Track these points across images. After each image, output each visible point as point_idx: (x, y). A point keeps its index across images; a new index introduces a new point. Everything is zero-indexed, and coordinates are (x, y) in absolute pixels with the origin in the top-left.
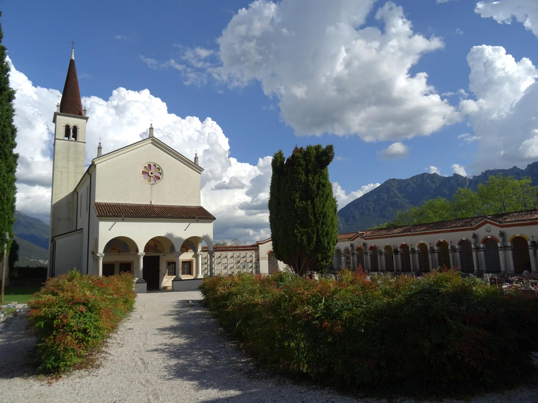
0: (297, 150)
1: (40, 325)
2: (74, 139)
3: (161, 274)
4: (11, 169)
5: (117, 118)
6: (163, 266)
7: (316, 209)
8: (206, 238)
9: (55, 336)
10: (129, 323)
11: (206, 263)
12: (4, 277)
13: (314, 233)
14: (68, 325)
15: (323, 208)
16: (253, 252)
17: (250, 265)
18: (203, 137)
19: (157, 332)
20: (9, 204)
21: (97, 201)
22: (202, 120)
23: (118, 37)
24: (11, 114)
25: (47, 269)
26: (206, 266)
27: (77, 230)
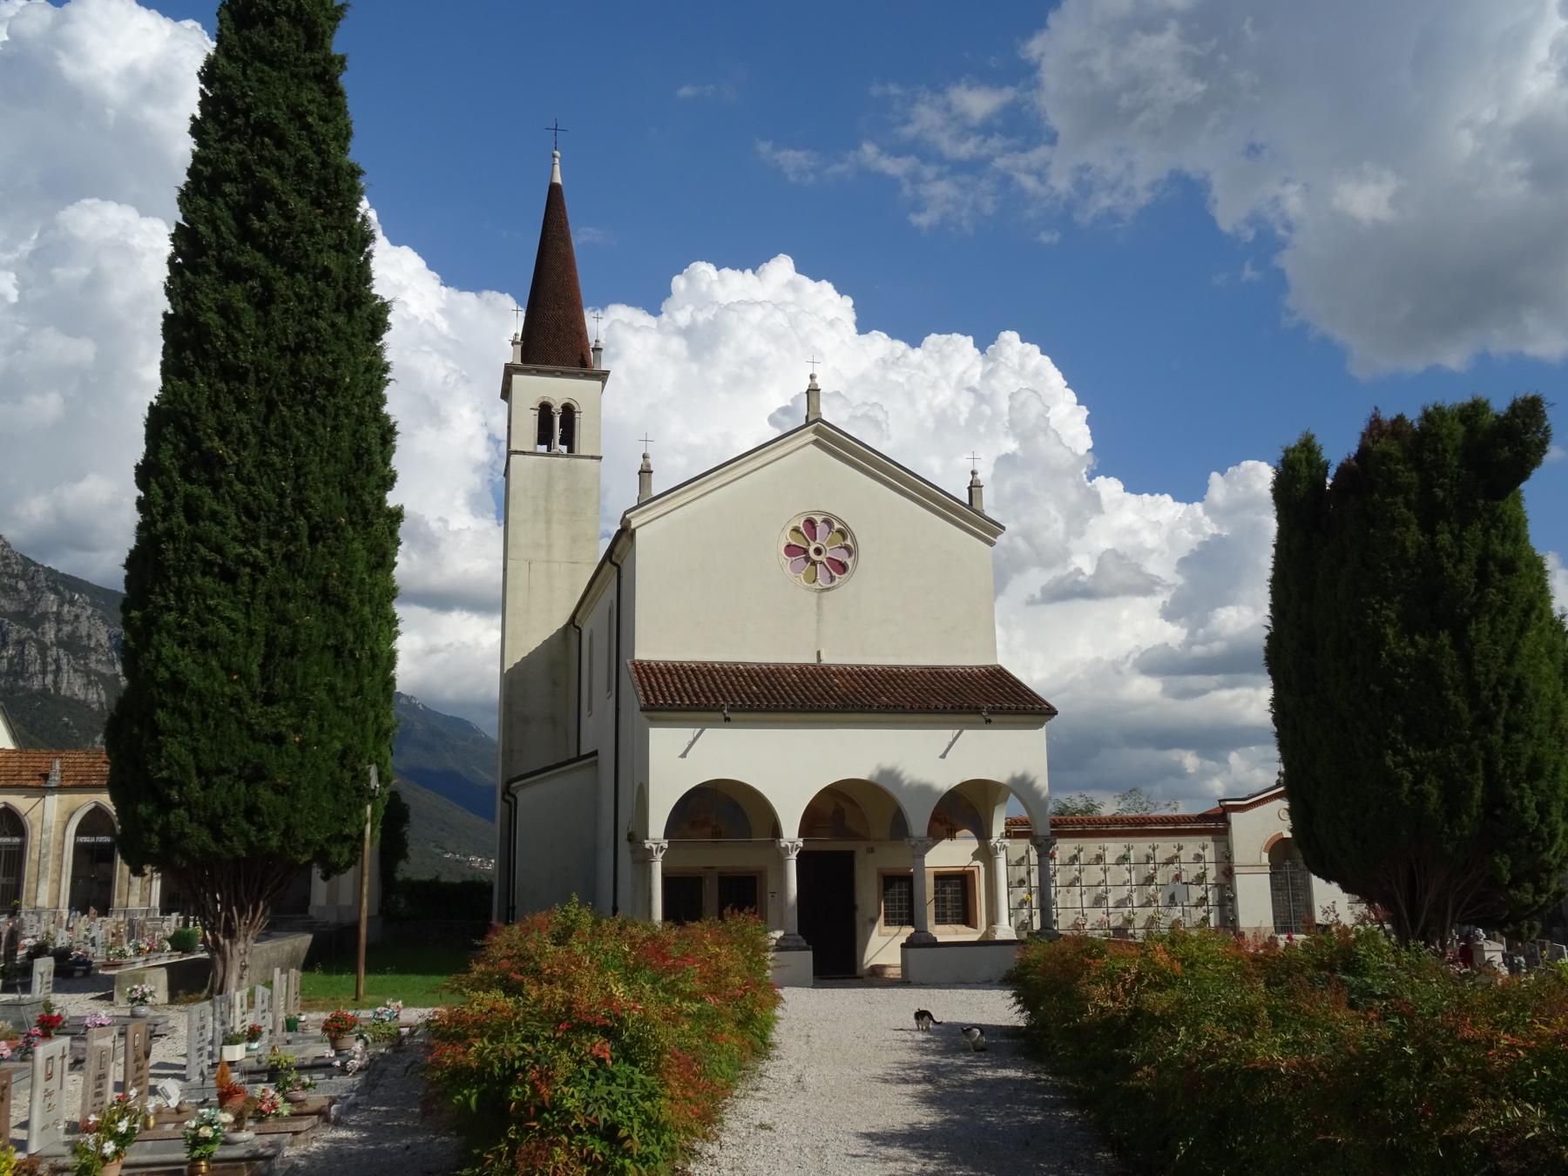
0: (1376, 428)
1: (467, 1099)
2: (564, 449)
3: (860, 919)
4: (383, 561)
5: (694, 368)
6: (867, 891)
8: (1021, 787)
9: (513, 1144)
10: (760, 1104)
11: (1021, 882)
12: (364, 915)
13: (1472, 768)
14: (555, 1106)
15: (1510, 660)
16: (1208, 840)
17: (1196, 892)
18: (987, 410)
19: (860, 1147)
20: (377, 672)
21: (641, 655)
22: (984, 342)
23: (686, 91)
24: (380, 378)
25: (491, 887)
26: (1022, 893)
27: (580, 758)
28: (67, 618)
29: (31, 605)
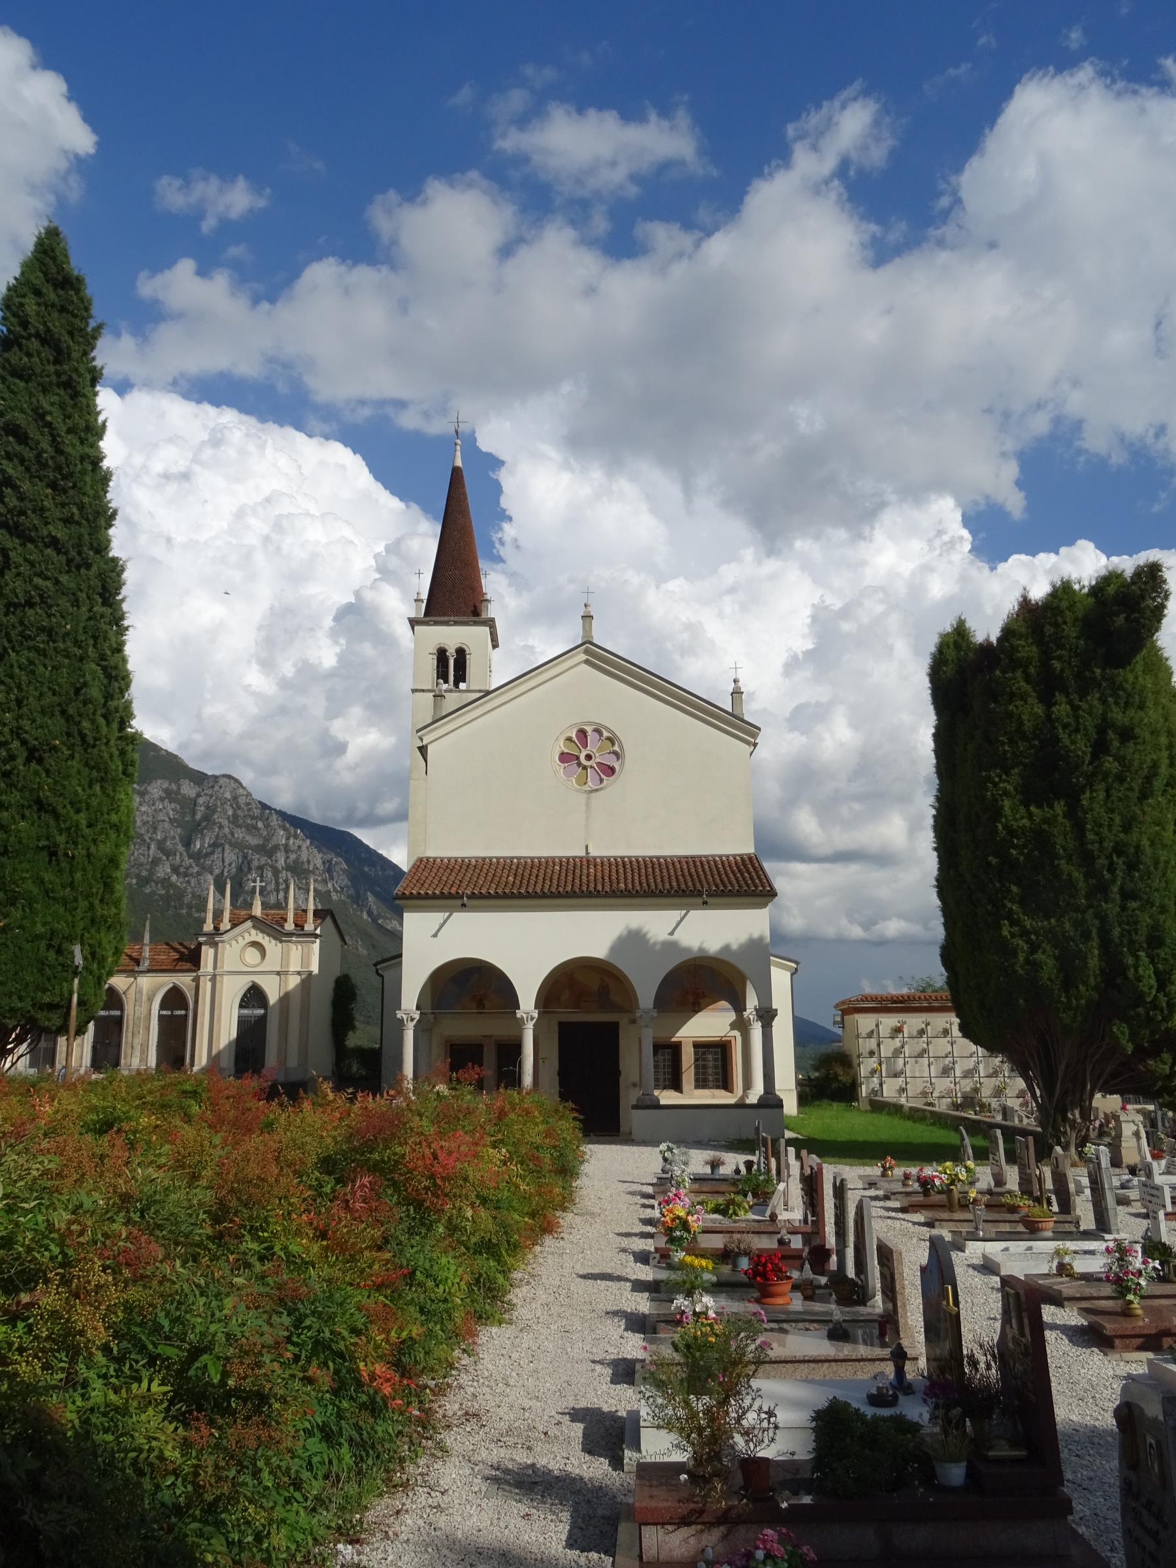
7: (1090, 836)
13: (1086, 936)
15: (1127, 828)
28: (292, 848)
29: (267, 839)
